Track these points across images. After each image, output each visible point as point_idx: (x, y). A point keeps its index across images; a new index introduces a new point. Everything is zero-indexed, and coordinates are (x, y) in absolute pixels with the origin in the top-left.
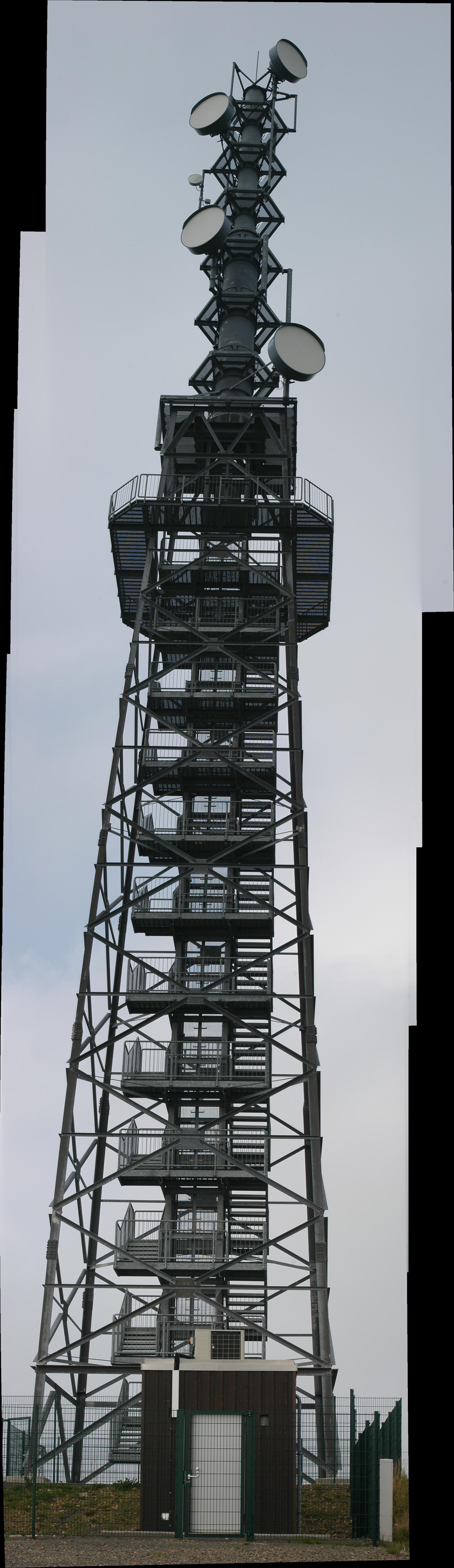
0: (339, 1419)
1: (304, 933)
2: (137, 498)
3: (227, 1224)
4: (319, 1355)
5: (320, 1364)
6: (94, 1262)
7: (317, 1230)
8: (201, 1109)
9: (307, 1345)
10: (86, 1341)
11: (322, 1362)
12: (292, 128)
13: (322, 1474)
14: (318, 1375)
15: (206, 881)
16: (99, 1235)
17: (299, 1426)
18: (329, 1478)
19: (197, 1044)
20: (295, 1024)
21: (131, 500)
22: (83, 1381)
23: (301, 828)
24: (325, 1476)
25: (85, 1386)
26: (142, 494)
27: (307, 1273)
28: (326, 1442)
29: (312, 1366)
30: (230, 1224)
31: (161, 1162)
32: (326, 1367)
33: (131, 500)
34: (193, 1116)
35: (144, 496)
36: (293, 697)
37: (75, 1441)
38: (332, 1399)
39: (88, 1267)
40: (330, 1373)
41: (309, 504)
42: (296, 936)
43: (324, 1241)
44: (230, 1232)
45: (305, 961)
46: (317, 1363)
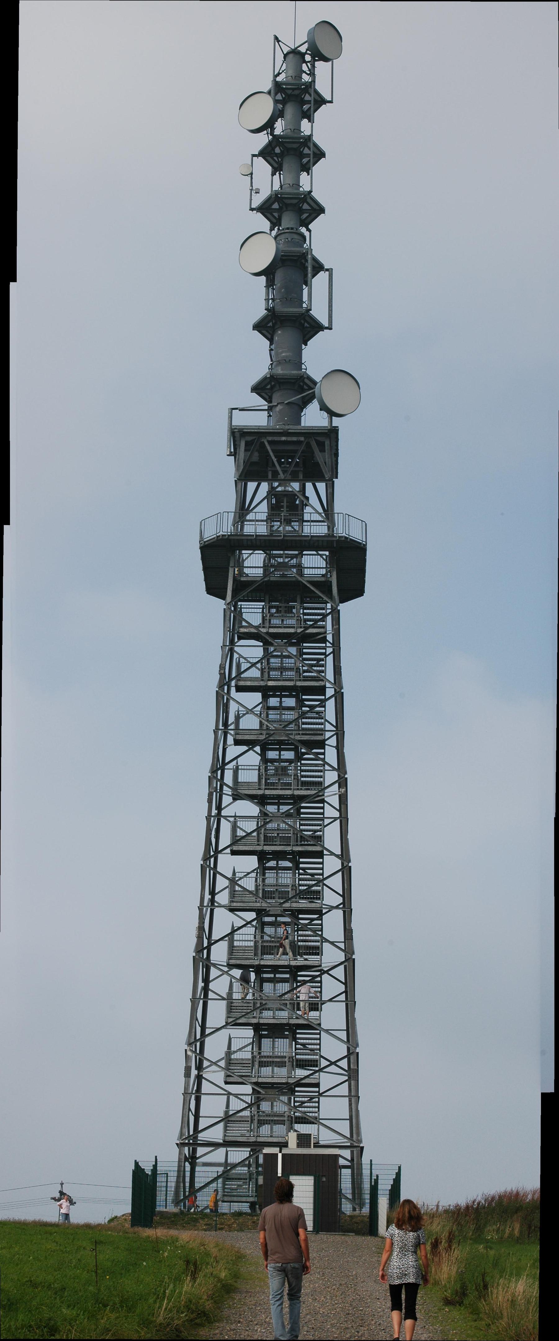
0: (364, 1167)
1: (345, 865)
2: (221, 533)
3: (296, 936)
4: (353, 1137)
5: (353, 1143)
6: (202, 1069)
7: (352, 1061)
8: (282, 753)
9: (345, 1128)
10: (216, 855)
11: (354, 1141)
12: (329, 99)
13: (354, 1209)
14: (352, 1149)
15: (281, 716)
16: (218, 870)
17: (341, 1175)
18: (357, 1212)
19: (280, 659)
20: (337, 907)
21: (217, 534)
22: (194, 1151)
23: (343, 790)
24: (355, 1211)
25: (196, 1153)
26: (225, 530)
27: (347, 1078)
28: (356, 1195)
29: (349, 1144)
30: (296, 1045)
31: (256, 841)
32: (357, 1145)
33: (217, 534)
34: (278, 705)
35: (226, 531)
36: (338, 690)
37: (215, 856)
38: (360, 1165)
39: (198, 1073)
40: (359, 1149)
41: (349, 535)
42: (340, 868)
43: (356, 1067)
44: (296, 1054)
45: (345, 876)
46: (352, 1142)
